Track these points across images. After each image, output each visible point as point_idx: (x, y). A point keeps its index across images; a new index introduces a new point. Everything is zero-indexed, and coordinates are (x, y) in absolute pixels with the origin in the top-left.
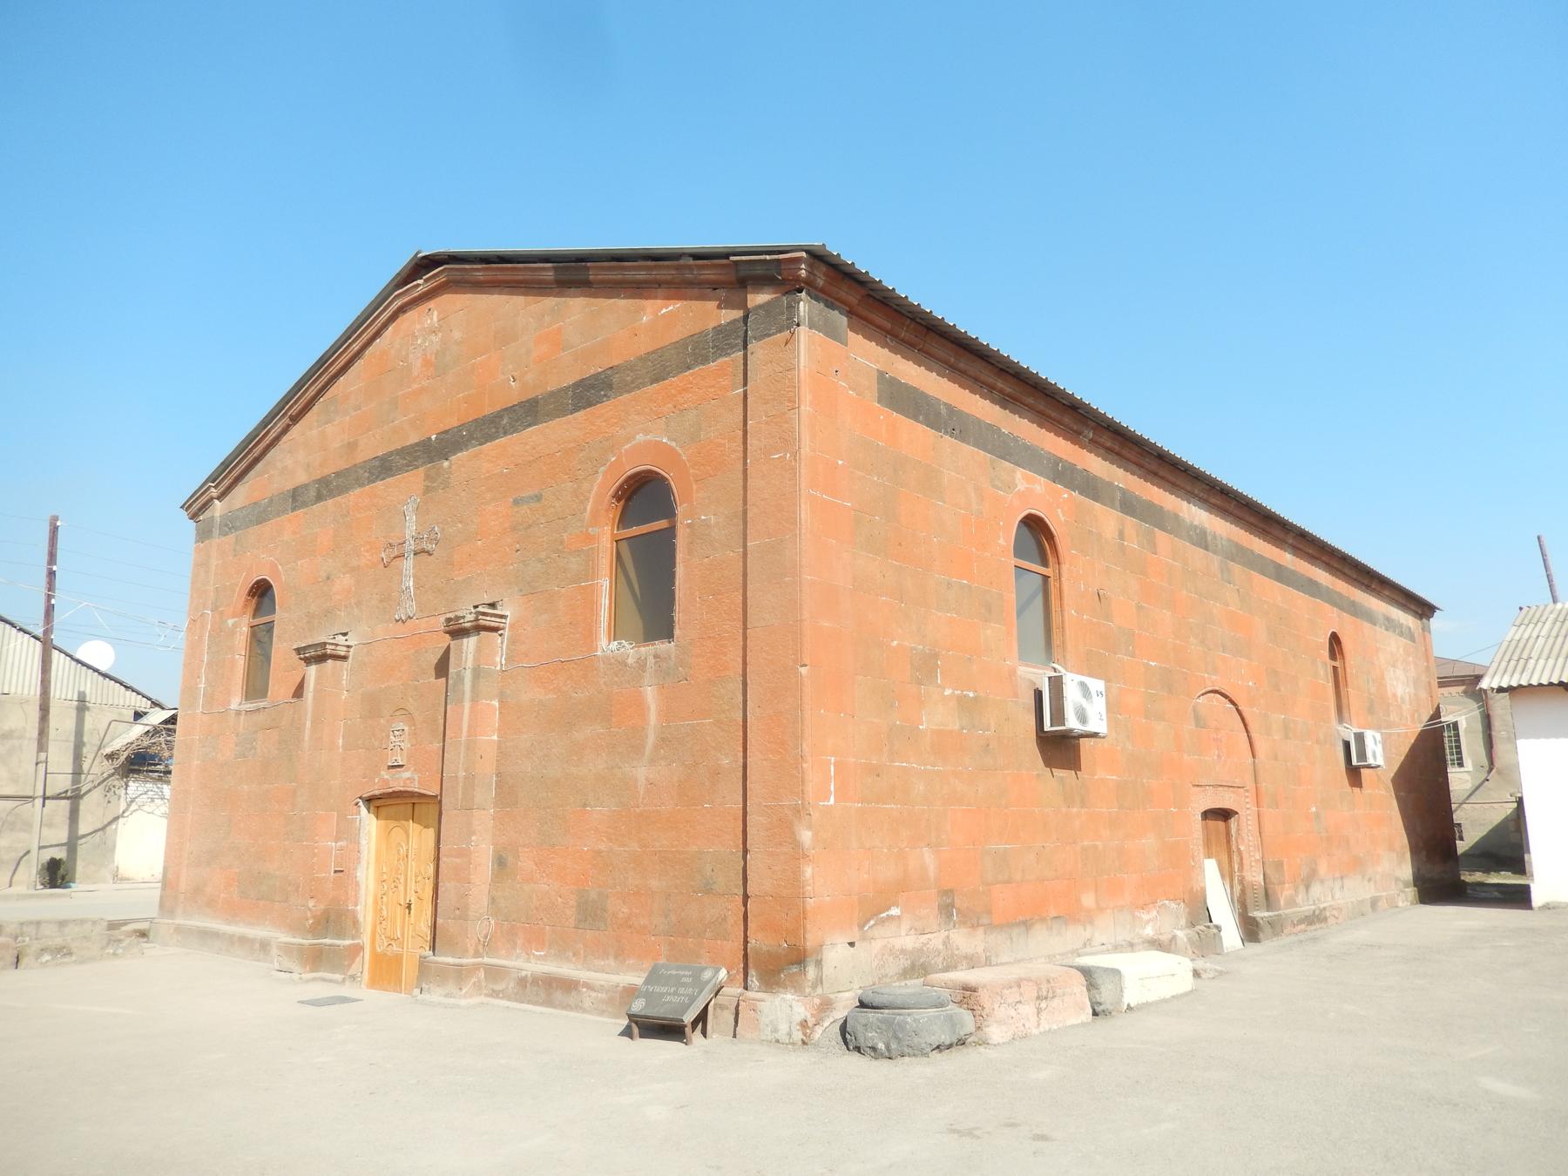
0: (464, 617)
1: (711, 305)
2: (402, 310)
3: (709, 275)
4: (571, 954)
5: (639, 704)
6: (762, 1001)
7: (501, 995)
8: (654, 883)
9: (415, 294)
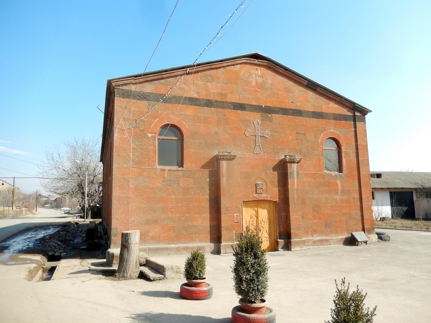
0: (296, 159)
1: (346, 110)
2: (245, 63)
3: (348, 105)
4: (324, 234)
5: (337, 184)
6: (370, 236)
7: (308, 246)
8: (343, 219)
9: (253, 62)
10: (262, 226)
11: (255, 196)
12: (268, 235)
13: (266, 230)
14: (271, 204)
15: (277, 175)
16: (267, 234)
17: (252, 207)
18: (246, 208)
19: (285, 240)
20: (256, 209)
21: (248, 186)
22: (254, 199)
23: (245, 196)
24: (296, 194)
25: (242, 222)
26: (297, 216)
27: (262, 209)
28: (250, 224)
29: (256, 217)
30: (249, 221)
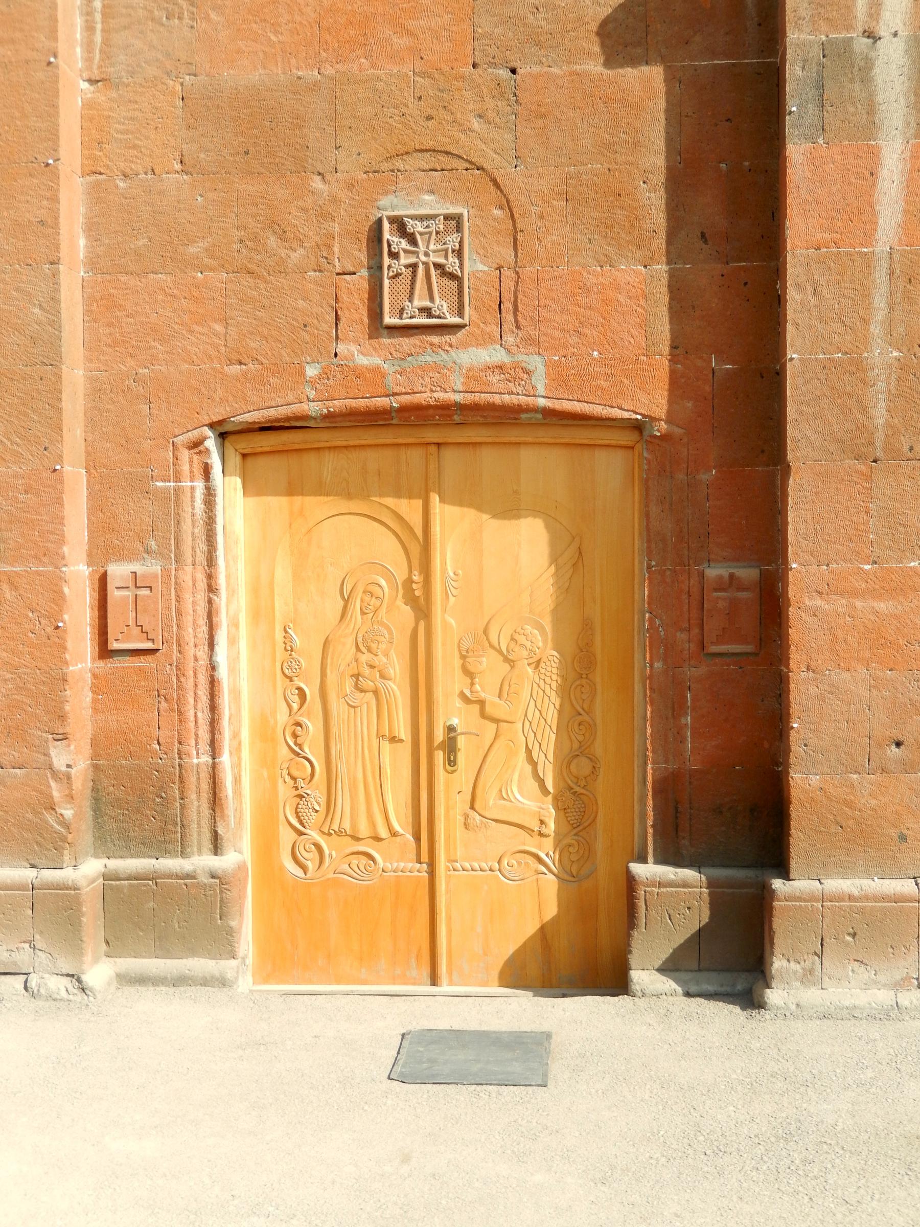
11: (362, 361)
13: (529, 752)
14: (601, 456)
15: (662, 103)
17: (364, 494)
18: (284, 500)
19: (711, 889)
20: (410, 509)
21: (283, 253)
22: (353, 403)
24: (889, 324)
25: (202, 653)
26: (882, 606)
27: (485, 517)
28: (332, 677)
29: (411, 599)
30: (326, 643)
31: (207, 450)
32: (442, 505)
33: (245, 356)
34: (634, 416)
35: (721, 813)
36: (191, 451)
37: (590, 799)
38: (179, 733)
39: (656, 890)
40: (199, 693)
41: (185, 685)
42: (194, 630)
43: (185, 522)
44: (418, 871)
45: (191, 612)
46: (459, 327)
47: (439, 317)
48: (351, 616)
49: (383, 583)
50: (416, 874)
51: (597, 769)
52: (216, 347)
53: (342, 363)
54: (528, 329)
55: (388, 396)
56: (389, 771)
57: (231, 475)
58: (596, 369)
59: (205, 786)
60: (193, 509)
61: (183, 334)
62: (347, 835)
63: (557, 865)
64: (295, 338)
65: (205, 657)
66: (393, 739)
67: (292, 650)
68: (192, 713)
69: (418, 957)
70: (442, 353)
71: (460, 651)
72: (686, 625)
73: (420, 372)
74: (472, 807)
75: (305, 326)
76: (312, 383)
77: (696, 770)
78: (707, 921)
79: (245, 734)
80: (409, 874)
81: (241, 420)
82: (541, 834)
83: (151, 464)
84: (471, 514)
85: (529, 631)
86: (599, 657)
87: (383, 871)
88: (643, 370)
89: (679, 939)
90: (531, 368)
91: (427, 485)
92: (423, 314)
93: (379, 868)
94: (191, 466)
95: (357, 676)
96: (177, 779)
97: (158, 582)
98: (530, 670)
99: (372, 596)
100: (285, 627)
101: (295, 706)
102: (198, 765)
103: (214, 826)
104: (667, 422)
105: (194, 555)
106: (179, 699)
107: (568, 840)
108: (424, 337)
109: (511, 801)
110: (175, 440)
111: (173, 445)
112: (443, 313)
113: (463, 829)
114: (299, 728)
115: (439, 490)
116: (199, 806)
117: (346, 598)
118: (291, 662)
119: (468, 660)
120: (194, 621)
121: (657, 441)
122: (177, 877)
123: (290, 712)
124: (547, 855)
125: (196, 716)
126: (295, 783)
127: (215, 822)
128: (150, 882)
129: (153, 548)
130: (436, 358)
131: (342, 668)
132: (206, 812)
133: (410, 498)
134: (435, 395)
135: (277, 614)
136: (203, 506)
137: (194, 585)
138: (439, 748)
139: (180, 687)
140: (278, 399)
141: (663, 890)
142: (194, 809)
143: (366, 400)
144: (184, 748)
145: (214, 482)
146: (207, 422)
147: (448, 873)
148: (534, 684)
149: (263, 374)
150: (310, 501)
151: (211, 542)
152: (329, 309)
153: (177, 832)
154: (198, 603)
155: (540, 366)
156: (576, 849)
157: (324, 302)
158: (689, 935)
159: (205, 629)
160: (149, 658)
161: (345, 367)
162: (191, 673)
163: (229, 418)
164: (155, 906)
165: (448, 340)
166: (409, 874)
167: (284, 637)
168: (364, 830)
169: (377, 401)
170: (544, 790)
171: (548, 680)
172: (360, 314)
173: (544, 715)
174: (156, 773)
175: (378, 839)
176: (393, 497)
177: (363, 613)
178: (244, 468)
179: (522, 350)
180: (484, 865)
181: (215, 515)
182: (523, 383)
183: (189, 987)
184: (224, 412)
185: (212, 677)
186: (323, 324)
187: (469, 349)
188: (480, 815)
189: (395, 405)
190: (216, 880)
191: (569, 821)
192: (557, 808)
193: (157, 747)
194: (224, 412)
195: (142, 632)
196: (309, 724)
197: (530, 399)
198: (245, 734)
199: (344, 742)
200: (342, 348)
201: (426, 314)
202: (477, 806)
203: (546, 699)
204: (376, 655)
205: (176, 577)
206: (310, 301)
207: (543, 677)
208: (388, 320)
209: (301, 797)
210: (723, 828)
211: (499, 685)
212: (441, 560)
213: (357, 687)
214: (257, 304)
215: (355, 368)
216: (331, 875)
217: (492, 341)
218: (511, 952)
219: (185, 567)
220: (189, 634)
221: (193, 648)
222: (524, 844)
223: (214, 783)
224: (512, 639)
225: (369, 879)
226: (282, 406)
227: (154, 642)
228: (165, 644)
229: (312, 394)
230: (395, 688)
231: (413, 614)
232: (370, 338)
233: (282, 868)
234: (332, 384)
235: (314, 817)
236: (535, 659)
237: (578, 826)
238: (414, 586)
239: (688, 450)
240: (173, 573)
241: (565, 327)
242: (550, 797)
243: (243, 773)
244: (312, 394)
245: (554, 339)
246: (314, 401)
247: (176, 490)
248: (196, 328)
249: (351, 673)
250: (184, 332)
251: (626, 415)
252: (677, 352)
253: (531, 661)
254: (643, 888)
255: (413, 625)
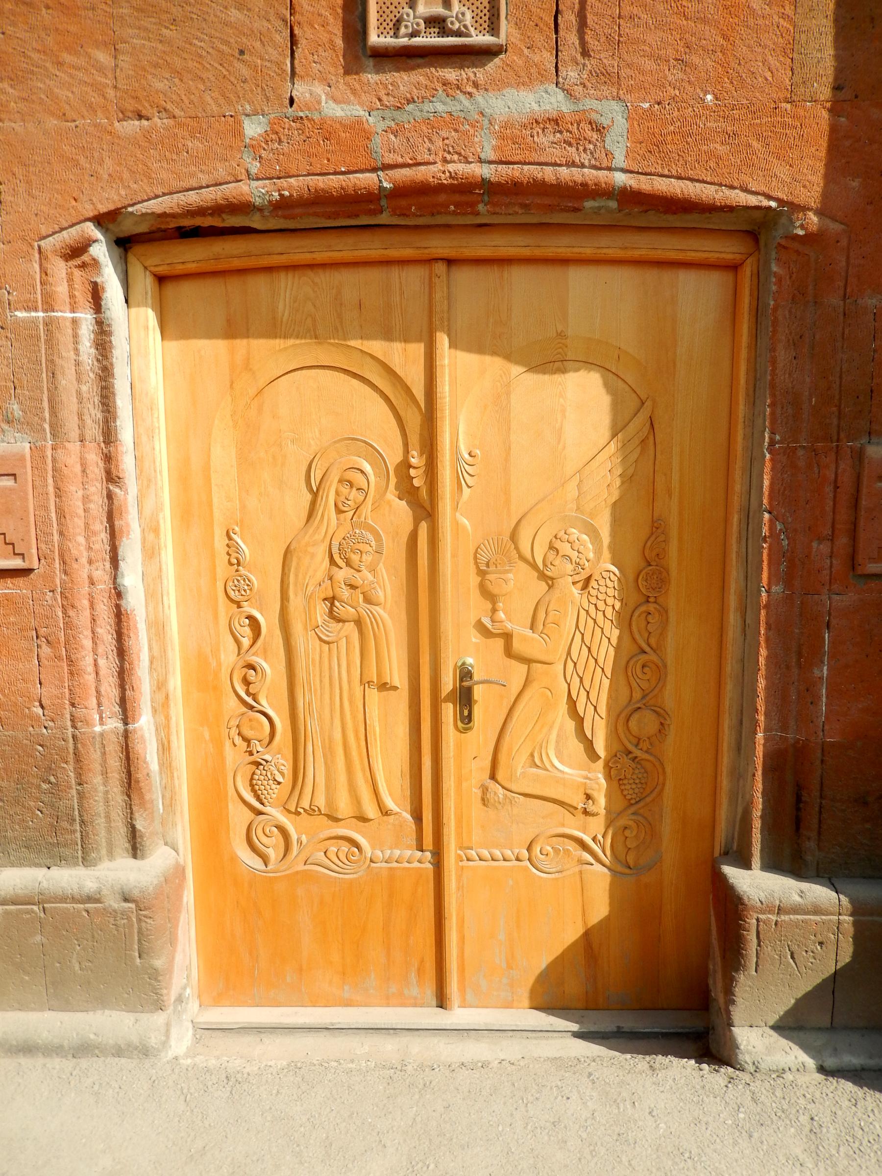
10: (507, 637)
11: (334, 110)
12: (608, 769)
13: (572, 704)
14: (687, 280)
16: (576, 747)
23: (133, 126)
25: (102, 572)
27: (516, 370)
28: (296, 602)
29: (408, 492)
30: (287, 553)
31: (95, 263)
32: (453, 351)
33: (147, 105)
34: (765, 203)
35: (866, 804)
36: (70, 263)
37: (655, 766)
38: (70, 690)
39: (774, 918)
40: (99, 630)
41: (75, 621)
42: (87, 539)
43: (63, 374)
44: (420, 861)
45: (81, 512)
46: (485, 53)
47: (458, 34)
48: (323, 516)
49: (367, 468)
50: (416, 865)
51: (666, 727)
52: (99, 89)
53: (301, 114)
54: (602, 56)
55: (374, 170)
56: (377, 729)
57: (139, 306)
58: (708, 124)
59: (115, 763)
60: (78, 354)
61: (46, 69)
62: (321, 814)
63: (609, 858)
64: (225, 73)
65: (107, 578)
66: (383, 687)
67: (239, 564)
68: (89, 660)
69: (420, 971)
70: (462, 97)
71: (476, 563)
72: (827, 531)
73: (426, 130)
74: (493, 777)
75: (242, 52)
76: (253, 147)
77: (832, 744)
78: (848, 960)
79: (176, 683)
80: (407, 865)
81: (144, 211)
82: (586, 812)
83: (6, 282)
84: (494, 364)
85: (576, 536)
86: (674, 573)
87: (371, 861)
88: (784, 125)
89: (805, 986)
90: (605, 122)
91: (430, 322)
92: (432, 30)
93: (365, 858)
94: (71, 286)
95: (331, 600)
96: (72, 756)
97: (25, 467)
98: (575, 591)
99: (352, 487)
100: (228, 532)
101: (246, 642)
102: (102, 735)
103: (131, 819)
104: (819, 213)
105: (82, 427)
106: (67, 642)
107: (622, 822)
108: (433, 70)
109: (547, 770)
110: (42, 243)
111: (40, 252)
112: (465, 26)
113: (481, 806)
114: (252, 672)
115: (449, 330)
116: (107, 792)
117: (315, 489)
118: (238, 581)
119: (488, 577)
120: (87, 525)
121: (796, 245)
122: (74, 900)
123: (239, 648)
124: (594, 839)
125: (96, 665)
126: (249, 746)
127: (132, 813)
128: (35, 908)
129: (16, 414)
130: (454, 107)
131: (310, 588)
132: (118, 797)
133: (406, 341)
134: (451, 167)
135: (217, 514)
136: (93, 351)
137: (84, 471)
138: (447, 699)
139: (69, 625)
140: (200, 175)
141: (784, 918)
142: (100, 797)
143: (341, 177)
144: (80, 712)
145: (108, 312)
146: (91, 214)
147: (460, 864)
148: (581, 610)
149: (176, 135)
150: (260, 346)
151: (108, 406)
152: (279, 24)
153: (74, 831)
154: (91, 498)
155: (620, 118)
156: (634, 833)
157: (272, 11)
158: (819, 981)
159: (104, 536)
160: (20, 581)
161: (306, 121)
162: (86, 603)
163: (125, 207)
164: (44, 940)
165: (472, 75)
166: (407, 865)
167: (228, 545)
168: (344, 807)
169: (358, 179)
170: (592, 754)
171: (601, 605)
172: (330, 33)
173: (594, 653)
174: (40, 748)
175: (363, 819)
176: (381, 339)
177: (339, 511)
178: (160, 295)
179: (592, 92)
180: (508, 853)
181: (112, 364)
182: (591, 147)
183: (96, 1059)
184: (116, 198)
185: (118, 607)
186: (270, 50)
187: (504, 92)
188: (503, 787)
189: (386, 184)
190: (130, 905)
191: (625, 796)
192: (608, 777)
193: (40, 711)
194: (116, 198)
195: (6, 544)
196: (265, 665)
197: (602, 175)
198: (176, 683)
199: (315, 690)
200: (301, 90)
201: (437, 30)
202: (500, 776)
203: (598, 631)
204: (360, 571)
205: (54, 460)
206: (249, 10)
207: (593, 600)
208: (375, 38)
209: (257, 764)
210: (868, 826)
211: (531, 613)
212: (451, 433)
213: (331, 614)
214: (164, 17)
215: (323, 122)
216: (301, 867)
217: (542, 77)
218: (544, 966)
219: (67, 444)
220: (78, 544)
221: (87, 565)
222: (563, 825)
223: (128, 758)
224: (551, 547)
225: (352, 871)
226: (208, 186)
227: (23, 558)
228: (43, 561)
229: (255, 167)
230: (385, 616)
231: (410, 513)
232: (347, 72)
233: (234, 858)
234: (286, 150)
235: (276, 791)
236: (584, 575)
237: (637, 802)
238: (412, 472)
239: (848, 258)
240: (49, 453)
241: (663, 52)
242: (600, 764)
243: (174, 738)
244: (255, 167)
245: (642, 72)
246: (258, 179)
247: (48, 323)
248: (67, 57)
249: (323, 596)
250: (48, 65)
251: (753, 201)
252: (841, 95)
253: (577, 578)
254: (755, 916)
255: (409, 527)
